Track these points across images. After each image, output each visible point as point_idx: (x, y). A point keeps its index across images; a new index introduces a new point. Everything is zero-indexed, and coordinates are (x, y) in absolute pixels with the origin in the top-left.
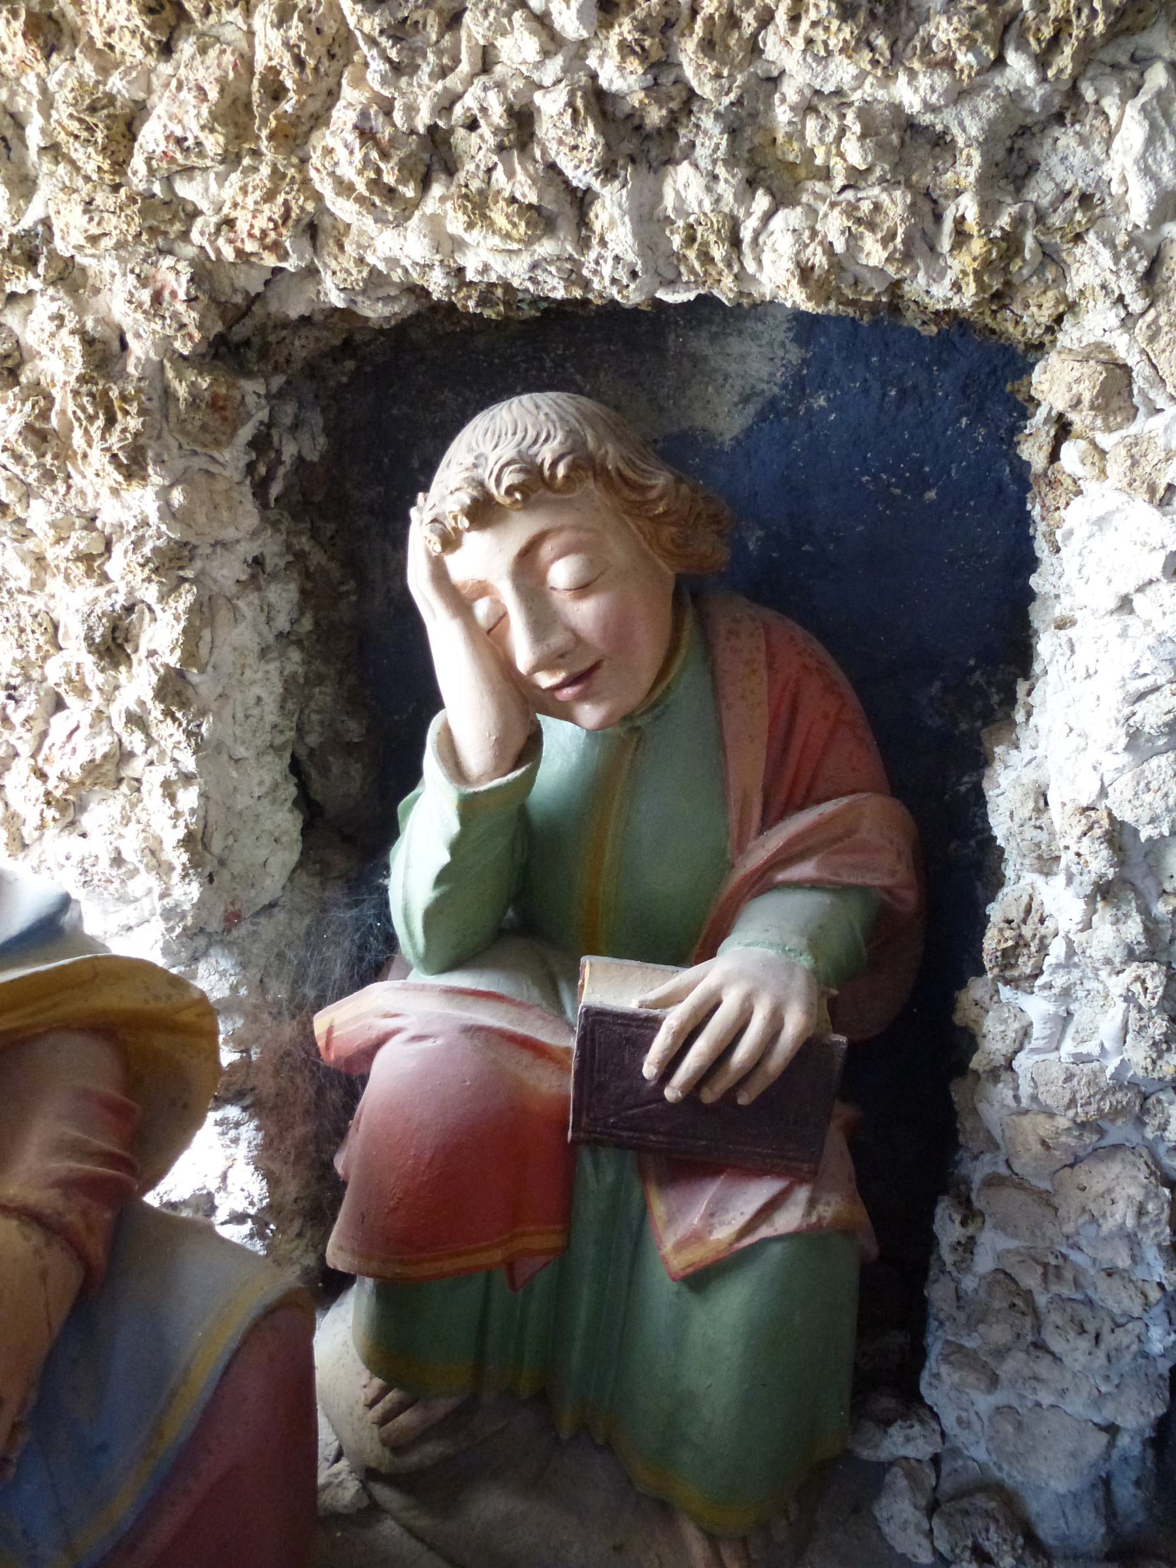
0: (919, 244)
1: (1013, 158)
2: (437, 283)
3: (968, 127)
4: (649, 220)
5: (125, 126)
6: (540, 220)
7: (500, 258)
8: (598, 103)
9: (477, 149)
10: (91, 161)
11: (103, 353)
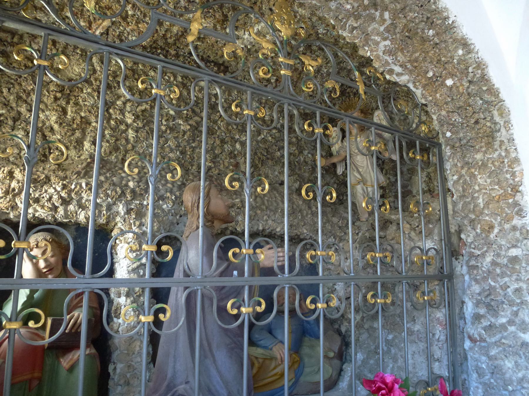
1: (109, 208)
3: (104, 204)
4: (66, 211)
8: (61, 197)
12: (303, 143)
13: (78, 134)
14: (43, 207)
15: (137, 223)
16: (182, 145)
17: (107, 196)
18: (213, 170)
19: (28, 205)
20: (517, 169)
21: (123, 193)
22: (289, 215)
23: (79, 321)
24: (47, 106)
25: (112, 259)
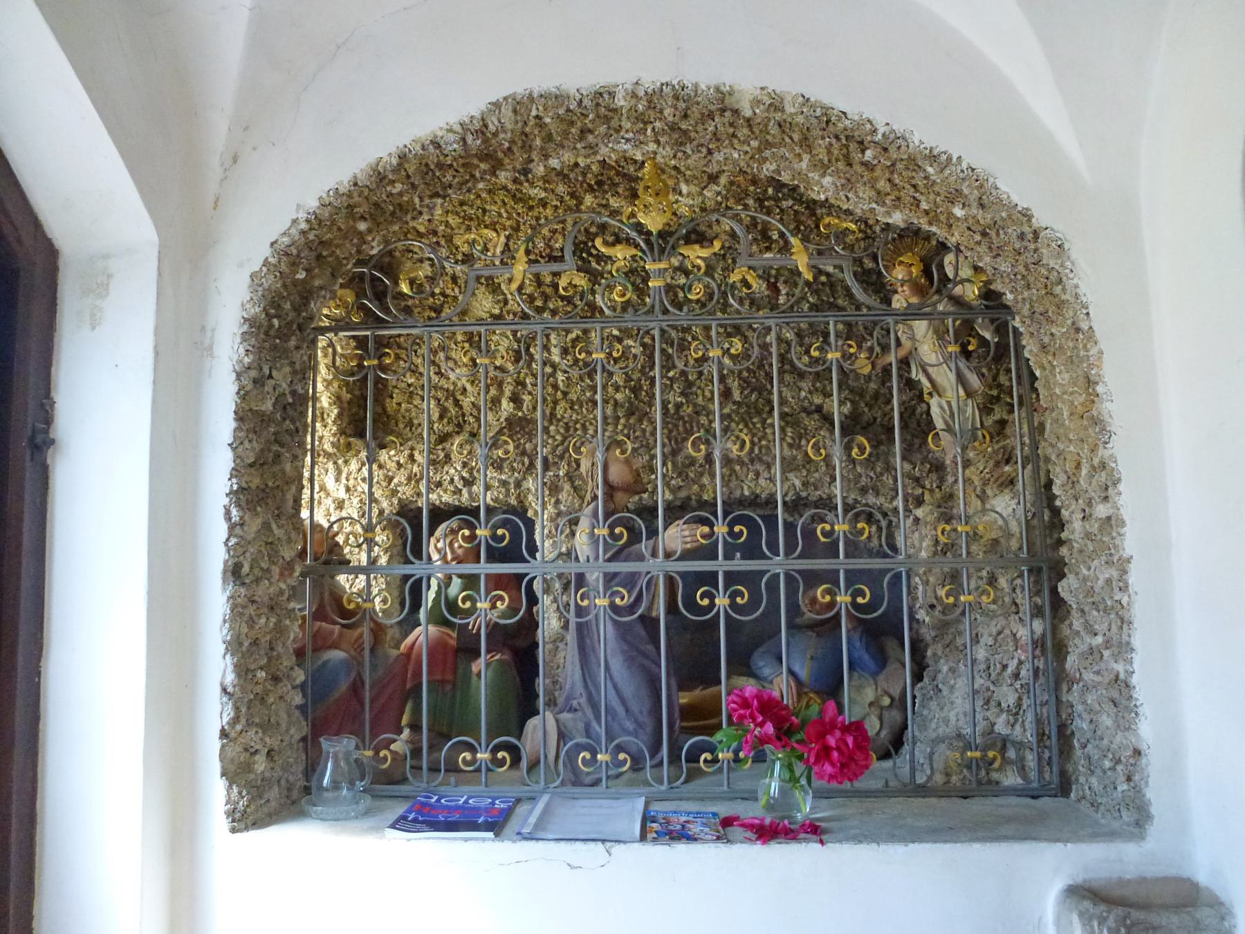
0: (507, 494)
1: (518, 484)
2: (437, 503)
3: (511, 481)
4: (470, 493)
5: (391, 479)
6: (454, 493)
7: (447, 498)
8: (463, 478)
9: (446, 483)
10: (384, 484)
11: (381, 512)
12: (861, 328)
13: (493, 392)
14: (445, 491)
15: (553, 500)
16: (634, 377)
17: (513, 469)
18: (685, 407)
19: (429, 490)
20: (326, 213)
21: (532, 465)
22: (901, 428)
23: (415, 651)
24: (456, 363)
25: (402, 592)
